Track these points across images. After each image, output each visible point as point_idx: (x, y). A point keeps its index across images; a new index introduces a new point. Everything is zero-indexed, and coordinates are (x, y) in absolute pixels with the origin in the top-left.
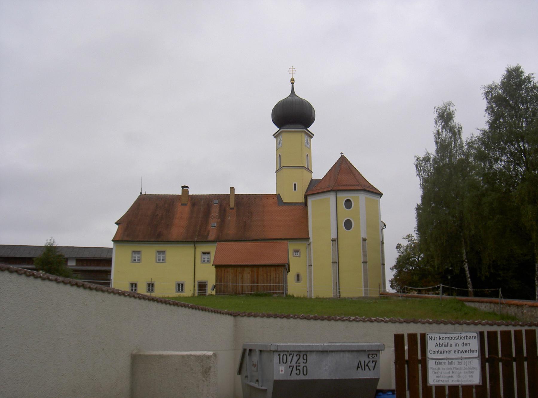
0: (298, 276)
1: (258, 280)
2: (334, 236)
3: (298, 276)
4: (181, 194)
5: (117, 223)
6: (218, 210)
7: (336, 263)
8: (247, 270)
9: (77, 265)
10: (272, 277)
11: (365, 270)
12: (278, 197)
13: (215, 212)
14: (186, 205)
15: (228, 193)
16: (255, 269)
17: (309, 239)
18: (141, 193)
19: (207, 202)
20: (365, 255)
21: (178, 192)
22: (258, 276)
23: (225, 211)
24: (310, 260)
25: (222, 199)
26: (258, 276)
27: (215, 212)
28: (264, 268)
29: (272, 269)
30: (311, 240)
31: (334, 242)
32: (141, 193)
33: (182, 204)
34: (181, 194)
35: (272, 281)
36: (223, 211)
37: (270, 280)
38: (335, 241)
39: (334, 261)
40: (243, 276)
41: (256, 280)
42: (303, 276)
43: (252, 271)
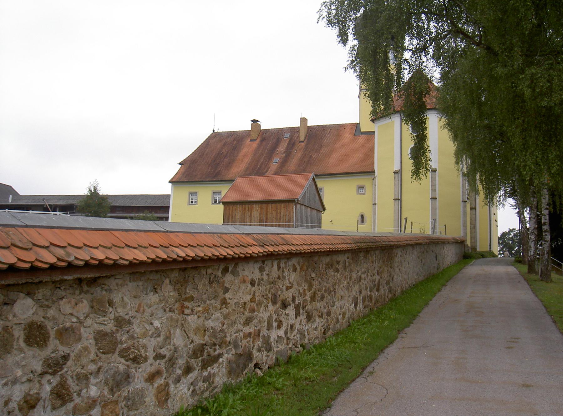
0: (362, 217)
1: (267, 219)
2: (397, 168)
3: (362, 217)
4: (250, 129)
5: (180, 164)
6: (286, 144)
7: (398, 200)
8: (256, 207)
9: (227, 220)
10: (282, 215)
11: (434, 209)
12: (357, 125)
13: (282, 147)
14: (255, 140)
15: (298, 124)
16: (264, 206)
17: (374, 172)
18: (214, 131)
19: (275, 136)
20: (434, 190)
21: (247, 127)
22: (267, 214)
23: (294, 144)
24: (375, 198)
25: (293, 131)
26: (267, 214)
27: (282, 147)
28: (274, 205)
29: (283, 205)
30: (376, 174)
31: (397, 175)
32: (214, 131)
33: (251, 140)
34: (250, 129)
35: (282, 219)
36: (292, 144)
37: (280, 219)
38: (397, 173)
39: (396, 198)
40: (251, 214)
41: (265, 218)
42: (367, 219)
43: (261, 208)
